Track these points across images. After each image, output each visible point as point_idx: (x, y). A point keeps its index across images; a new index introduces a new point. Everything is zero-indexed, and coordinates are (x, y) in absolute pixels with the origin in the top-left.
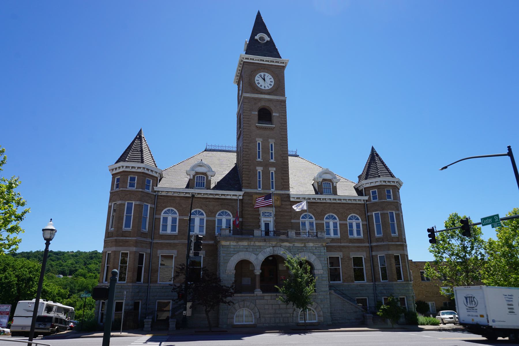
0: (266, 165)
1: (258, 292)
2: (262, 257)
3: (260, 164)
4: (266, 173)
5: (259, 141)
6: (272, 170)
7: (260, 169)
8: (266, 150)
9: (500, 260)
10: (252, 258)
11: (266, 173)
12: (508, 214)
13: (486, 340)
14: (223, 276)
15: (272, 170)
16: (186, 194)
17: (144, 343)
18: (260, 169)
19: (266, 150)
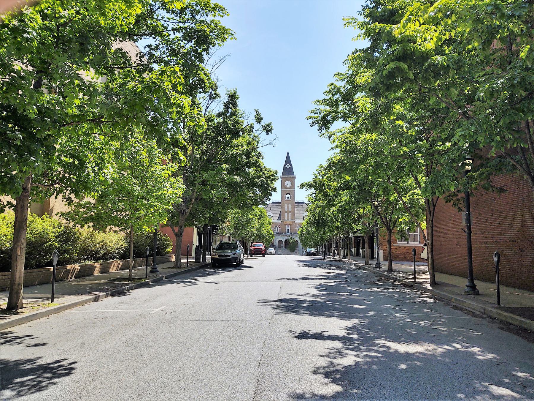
0: (288, 212)
1: (283, 248)
2: (285, 239)
3: (286, 212)
4: (288, 215)
5: (286, 204)
6: (290, 213)
7: (286, 213)
8: (288, 208)
9: (370, 157)
10: (282, 239)
11: (288, 215)
12: (264, 165)
13: (337, 395)
14: (275, 244)
15: (290, 213)
16: (85, 261)
17: (40, 358)
18: (286, 213)
19: (288, 208)
